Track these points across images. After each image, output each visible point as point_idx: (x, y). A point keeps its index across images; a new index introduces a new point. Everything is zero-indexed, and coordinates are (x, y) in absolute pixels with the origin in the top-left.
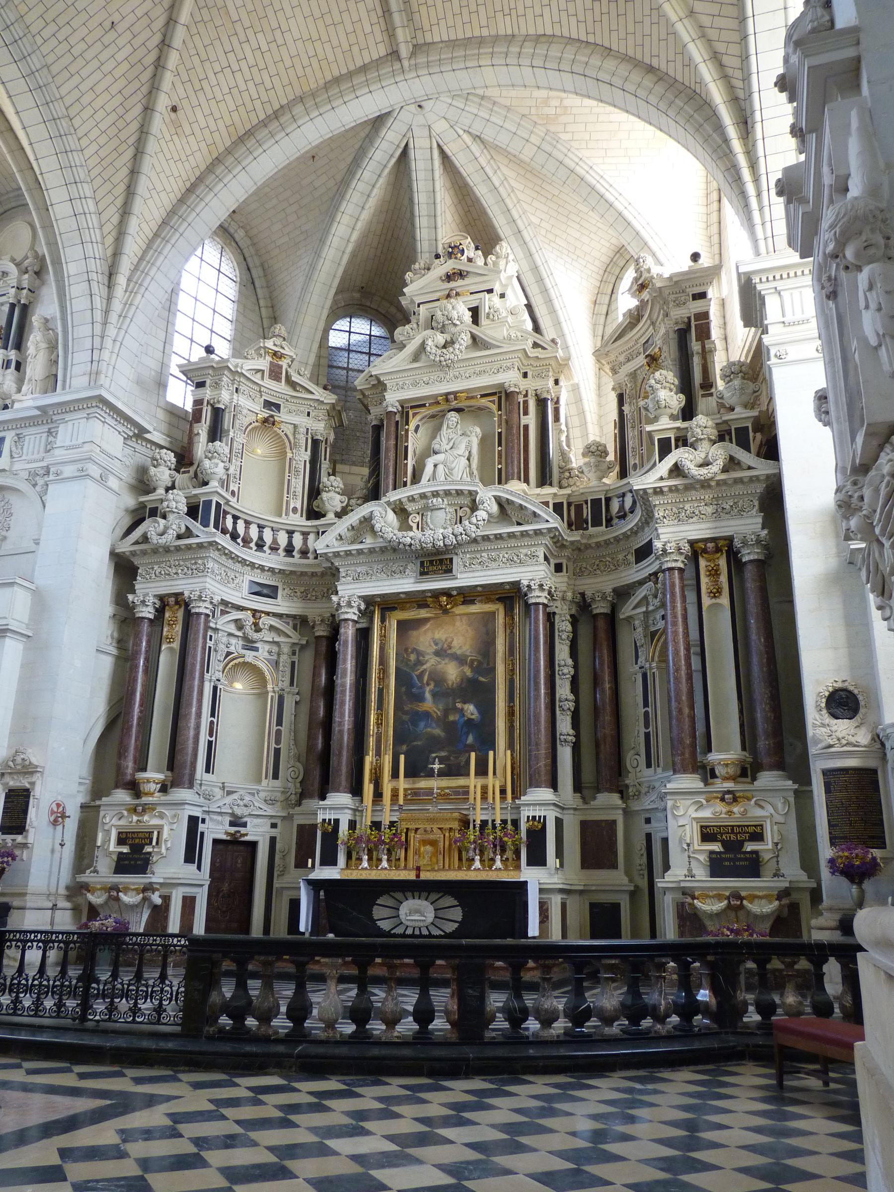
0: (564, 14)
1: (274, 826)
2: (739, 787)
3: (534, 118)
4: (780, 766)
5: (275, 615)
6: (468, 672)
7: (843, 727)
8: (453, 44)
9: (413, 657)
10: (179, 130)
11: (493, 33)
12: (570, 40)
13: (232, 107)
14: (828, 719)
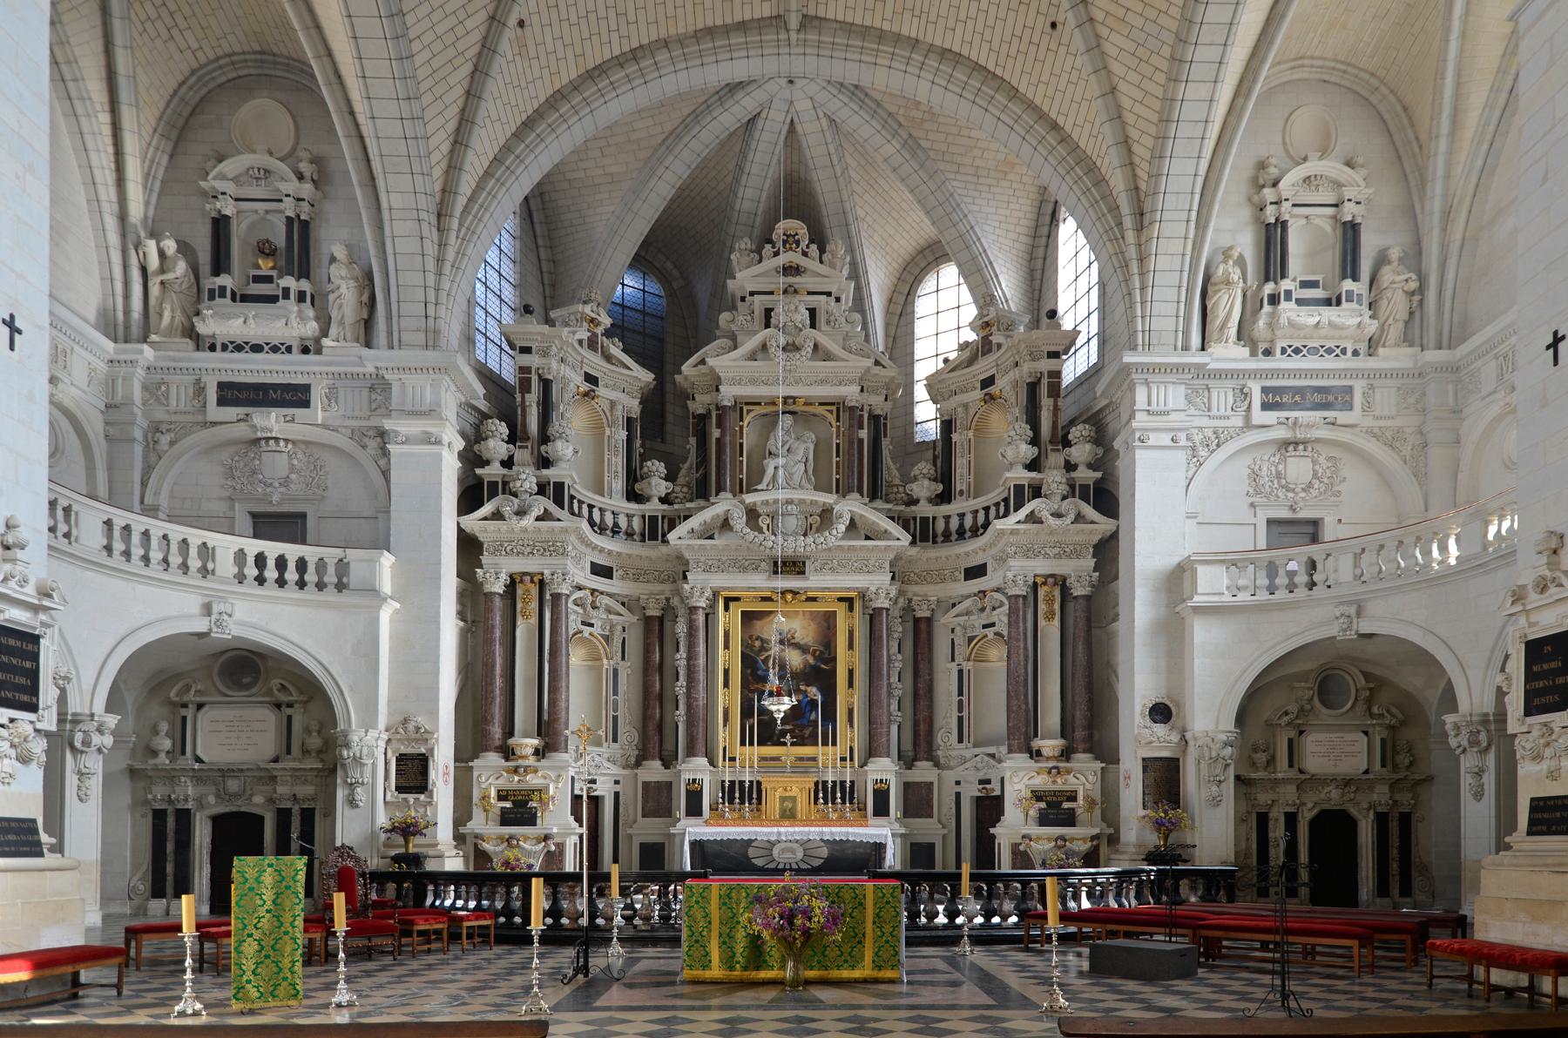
0: (977, 38)
1: (617, 782)
2: (1061, 765)
3: (901, 119)
5: (610, 595)
6: (812, 661)
7: (1160, 729)
8: (848, 28)
9: (757, 644)
10: (523, 50)
11: (895, 29)
12: (978, 67)
13: (586, 35)
14: (1148, 722)
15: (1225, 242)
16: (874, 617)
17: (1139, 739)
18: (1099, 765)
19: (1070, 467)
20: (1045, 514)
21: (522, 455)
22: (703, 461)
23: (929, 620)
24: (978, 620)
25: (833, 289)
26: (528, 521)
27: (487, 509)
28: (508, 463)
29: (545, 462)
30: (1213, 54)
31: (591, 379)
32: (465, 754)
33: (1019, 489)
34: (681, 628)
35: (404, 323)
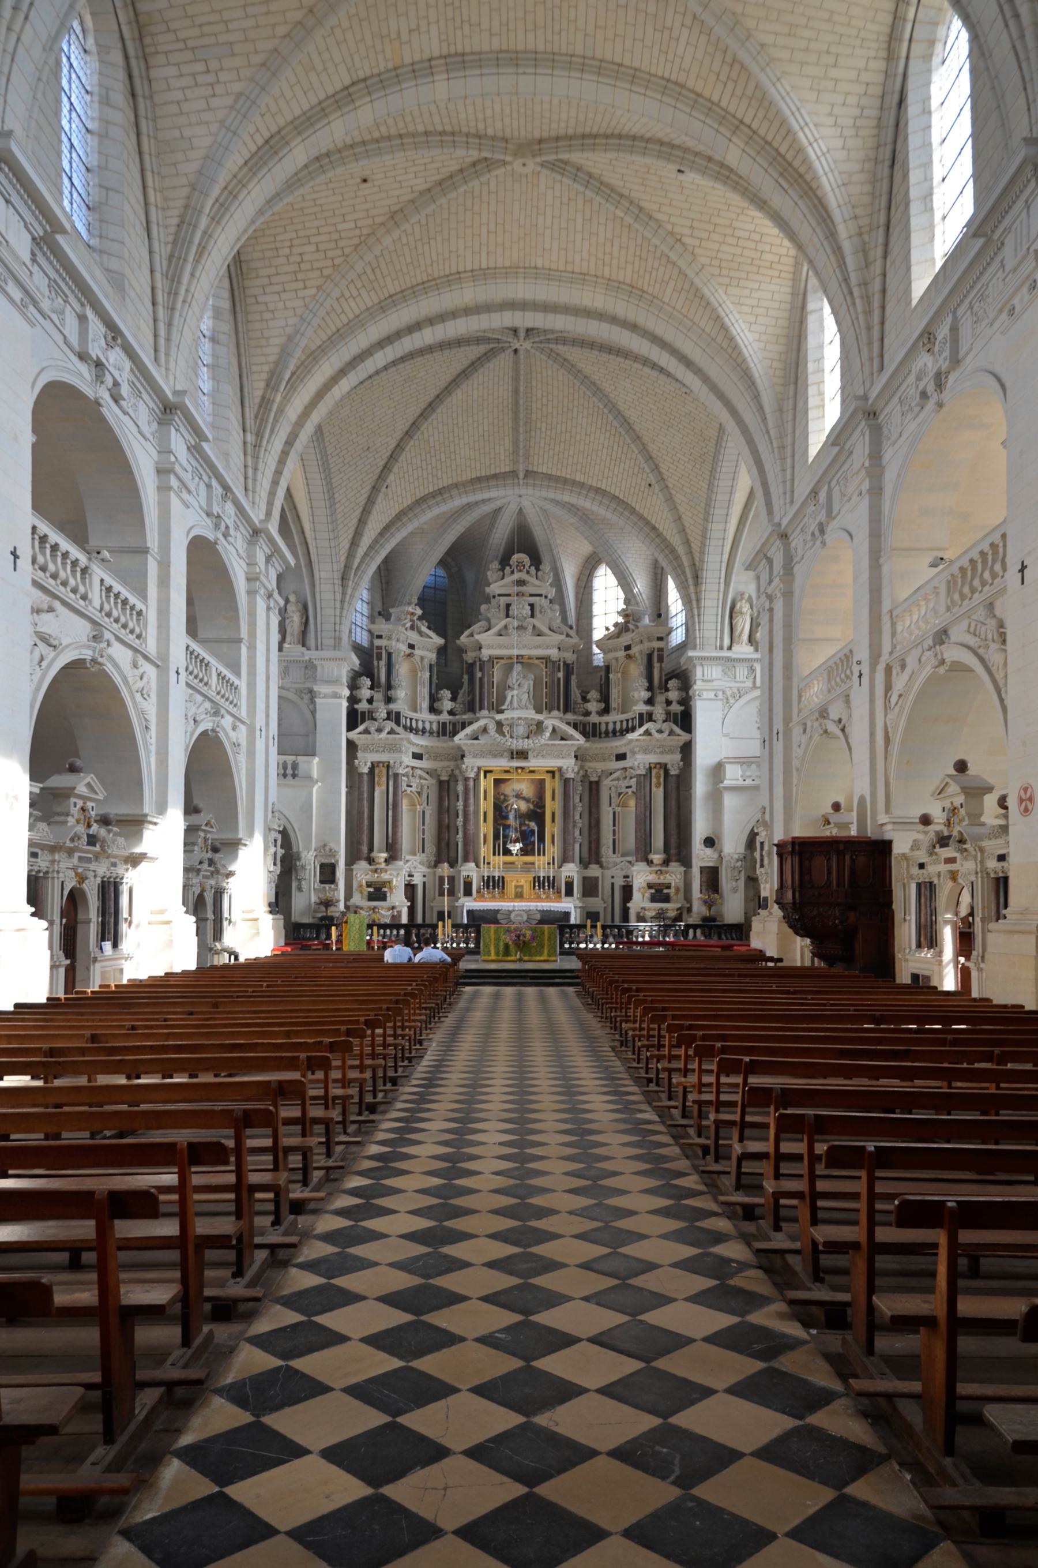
4: (678, 861)
7: (709, 851)
8: (549, 477)
15: (742, 588)
16: (566, 782)
17: (701, 856)
18: (683, 869)
19: (669, 703)
20: (653, 731)
21: (378, 696)
22: (472, 691)
23: (597, 783)
24: (624, 784)
25: (544, 593)
26: (383, 735)
27: (361, 728)
28: (370, 701)
29: (389, 700)
30: (721, 526)
31: (411, 646)
32: (350, 862)
33: (641, 715)
34: (460, 788)
35: (324, 634)
